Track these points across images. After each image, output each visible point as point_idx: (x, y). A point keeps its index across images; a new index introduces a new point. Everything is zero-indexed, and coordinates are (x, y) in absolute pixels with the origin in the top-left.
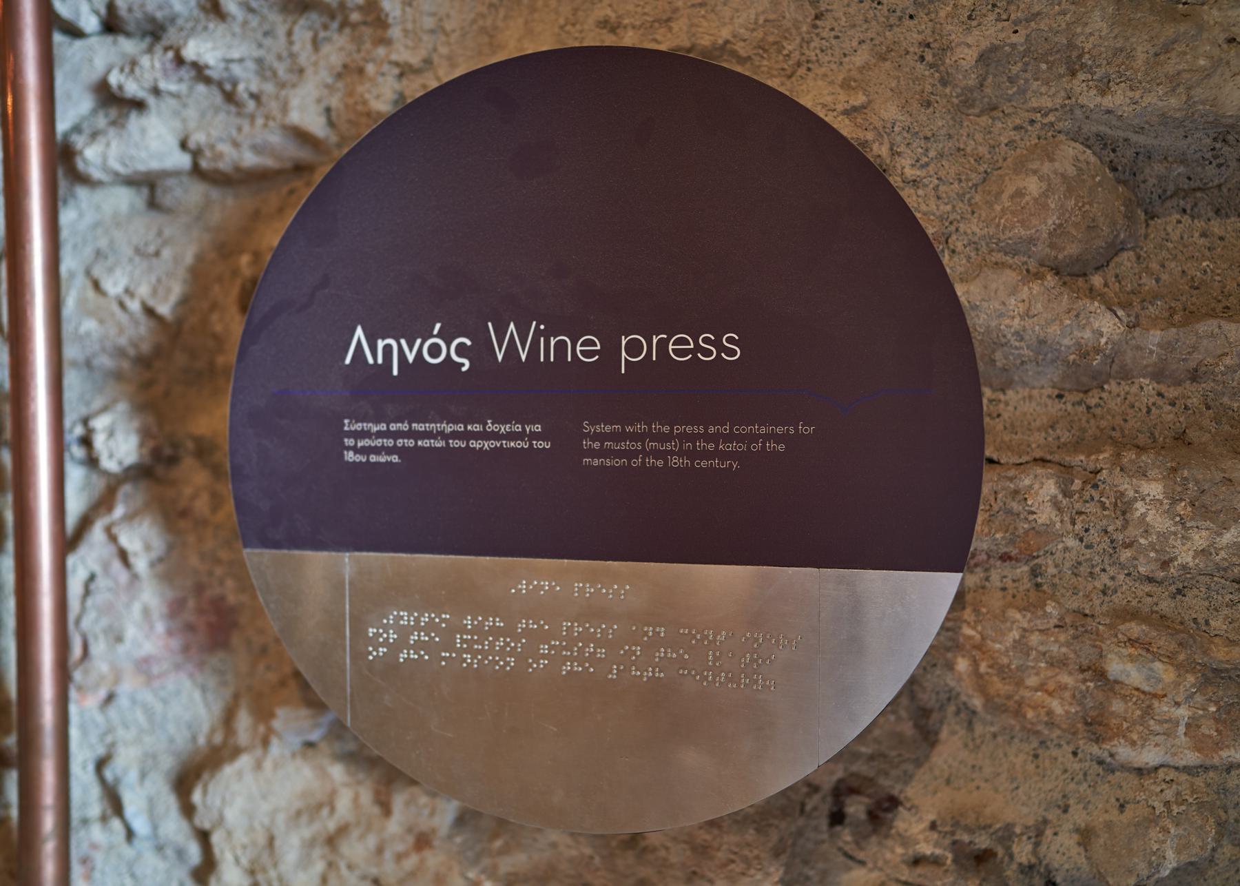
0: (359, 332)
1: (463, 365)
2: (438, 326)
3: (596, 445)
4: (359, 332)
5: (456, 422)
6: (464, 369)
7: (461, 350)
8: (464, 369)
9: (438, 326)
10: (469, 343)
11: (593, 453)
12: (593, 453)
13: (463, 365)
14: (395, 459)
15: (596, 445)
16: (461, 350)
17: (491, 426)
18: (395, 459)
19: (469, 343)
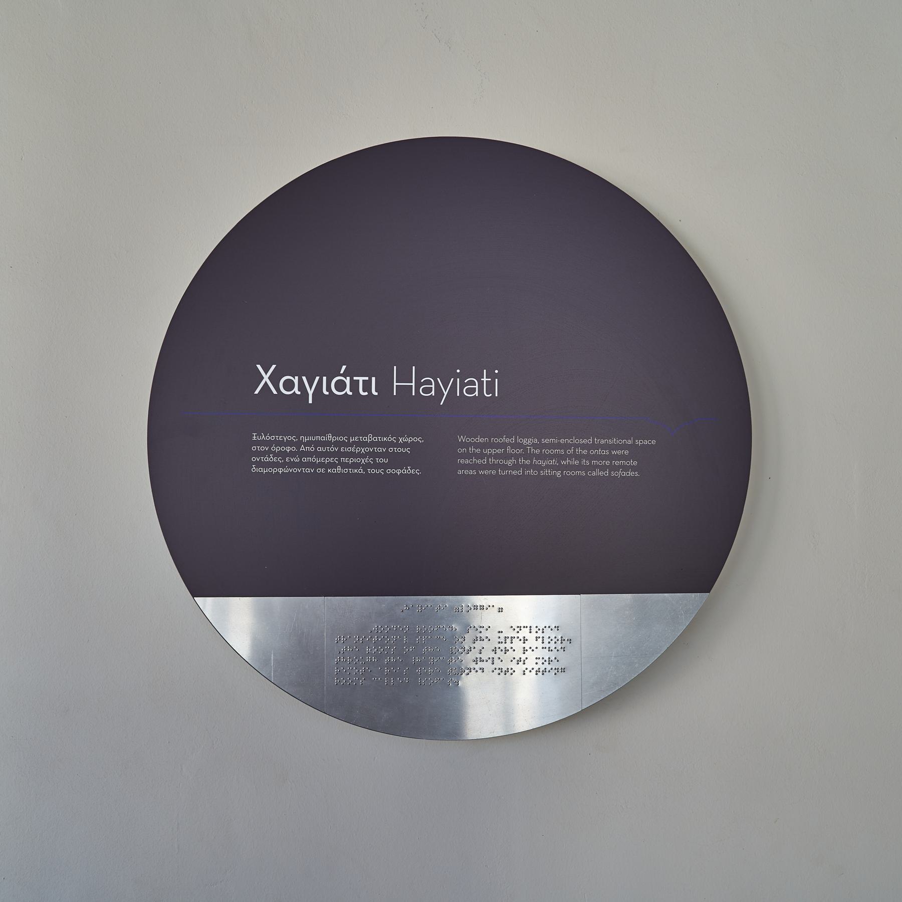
2: (344, 367)
3: (478, 451)
9: (344, 367)
18: (407, 450)
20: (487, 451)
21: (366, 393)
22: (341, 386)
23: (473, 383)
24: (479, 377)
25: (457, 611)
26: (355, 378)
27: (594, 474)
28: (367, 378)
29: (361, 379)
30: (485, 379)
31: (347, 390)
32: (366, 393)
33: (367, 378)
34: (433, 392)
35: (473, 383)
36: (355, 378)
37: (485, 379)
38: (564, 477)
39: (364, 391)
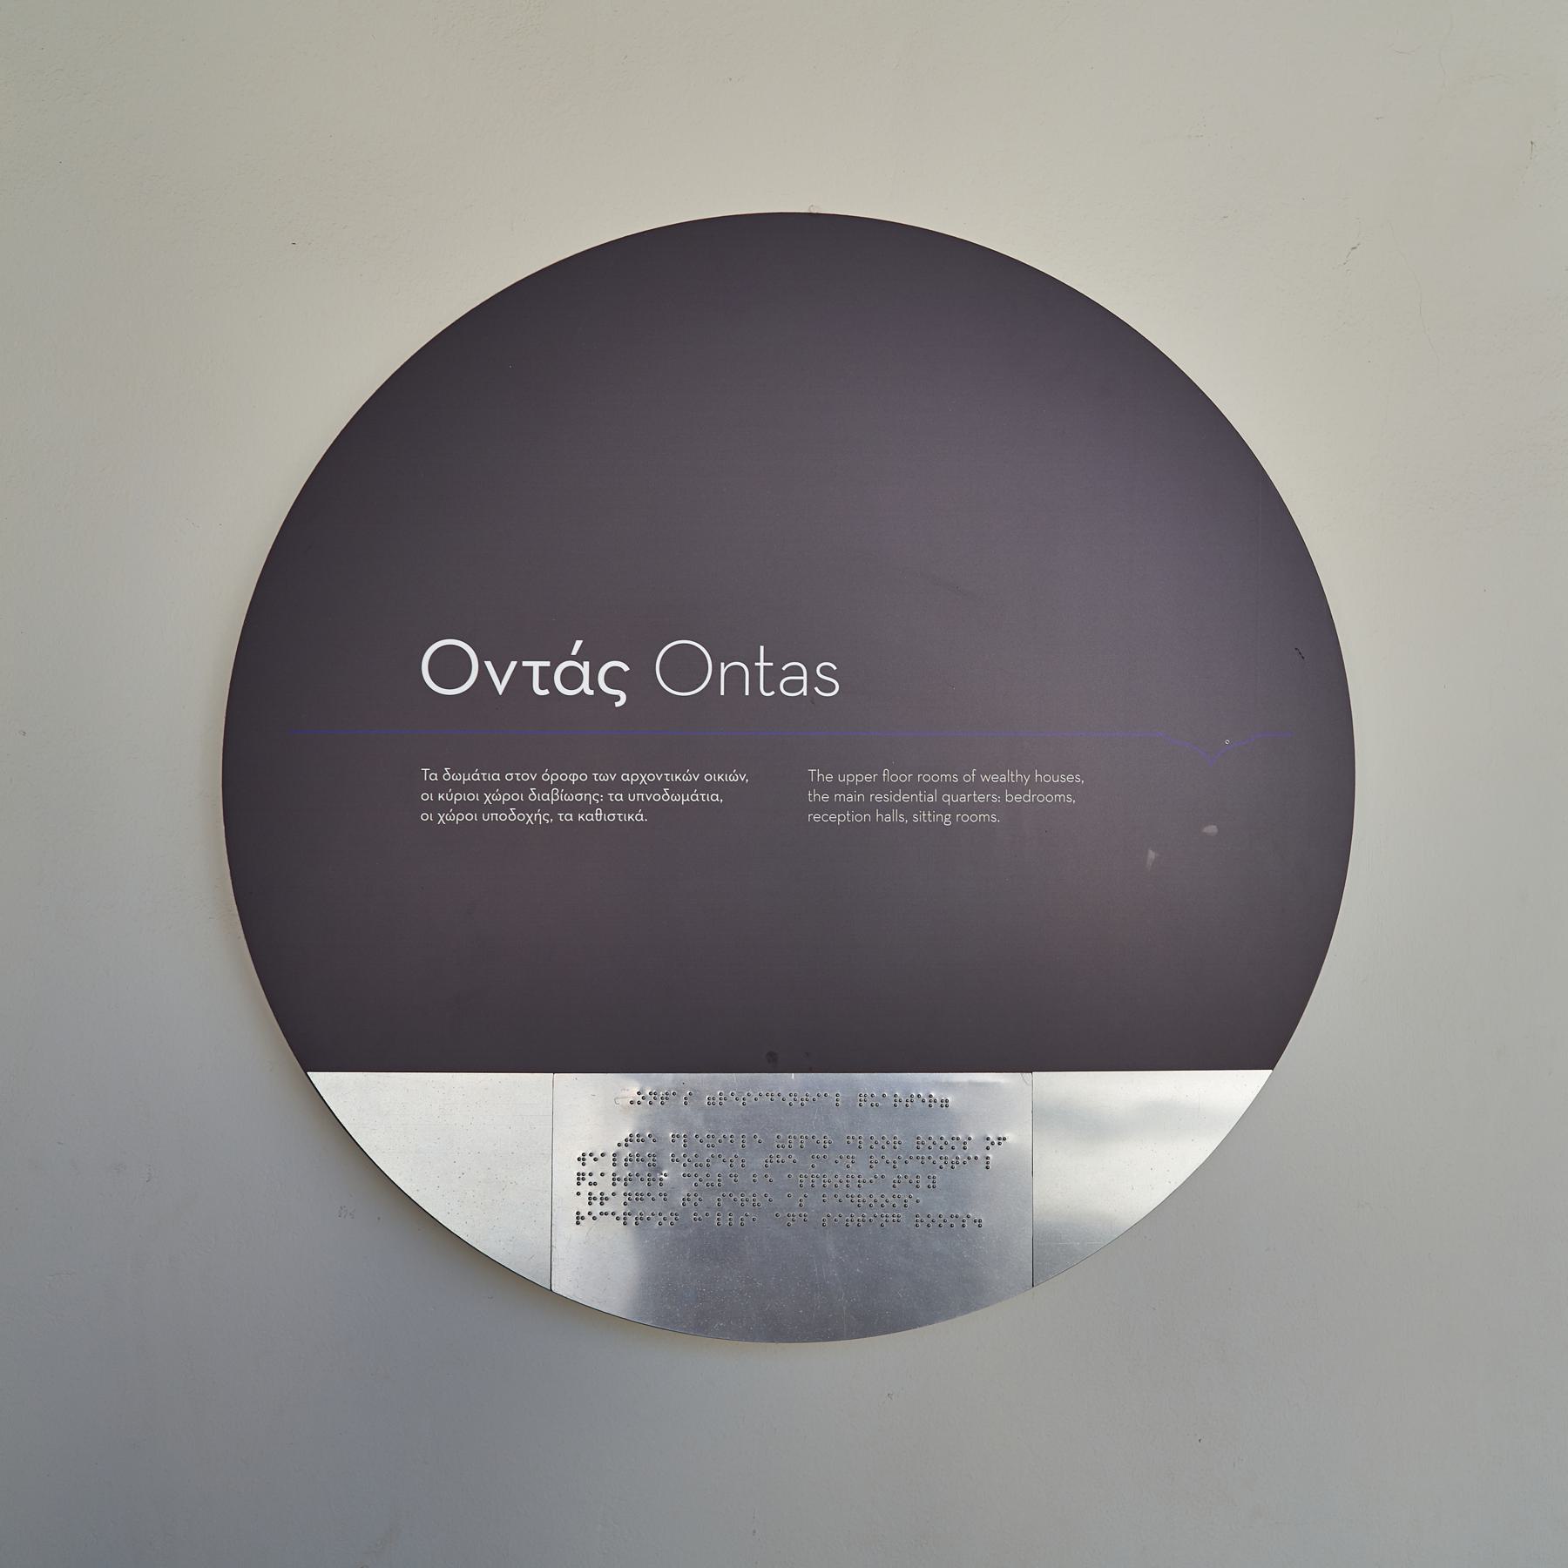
0: (500, 688)
1: (618, 698)
2: (578, 643)
3: (825, 798)
4: (500, 688)
5: (734, 705)
6: (618, 704)
7: (614, 678)
8: (618, 704)
9: (578, 643)
10: (626, 668)
11: (819, 807)
12: (819, 807)
13: (618, 698)
14: (716, 798)
15: (825, 798)
16: (614, 678)
17: (448, 775)
18: (716, 798)
19: (626, 668)
20: (948, 799)
21: (546, 692)
22: (572, 678)
23: (799, 672)
24: (751, 660)
25: (950, 1156)
26: (525, 664)
27: (888, 819)
28: (547, 664)
29: (536, 665)
30: (762, 664)
31: (585, 686)
32: (546, 692)
33: (547, 664)
34: (804, 690)
35: (799, 672)
36: (525, 664)
37: (762, 664)
38: (957, 825)
39: (542, 688)
